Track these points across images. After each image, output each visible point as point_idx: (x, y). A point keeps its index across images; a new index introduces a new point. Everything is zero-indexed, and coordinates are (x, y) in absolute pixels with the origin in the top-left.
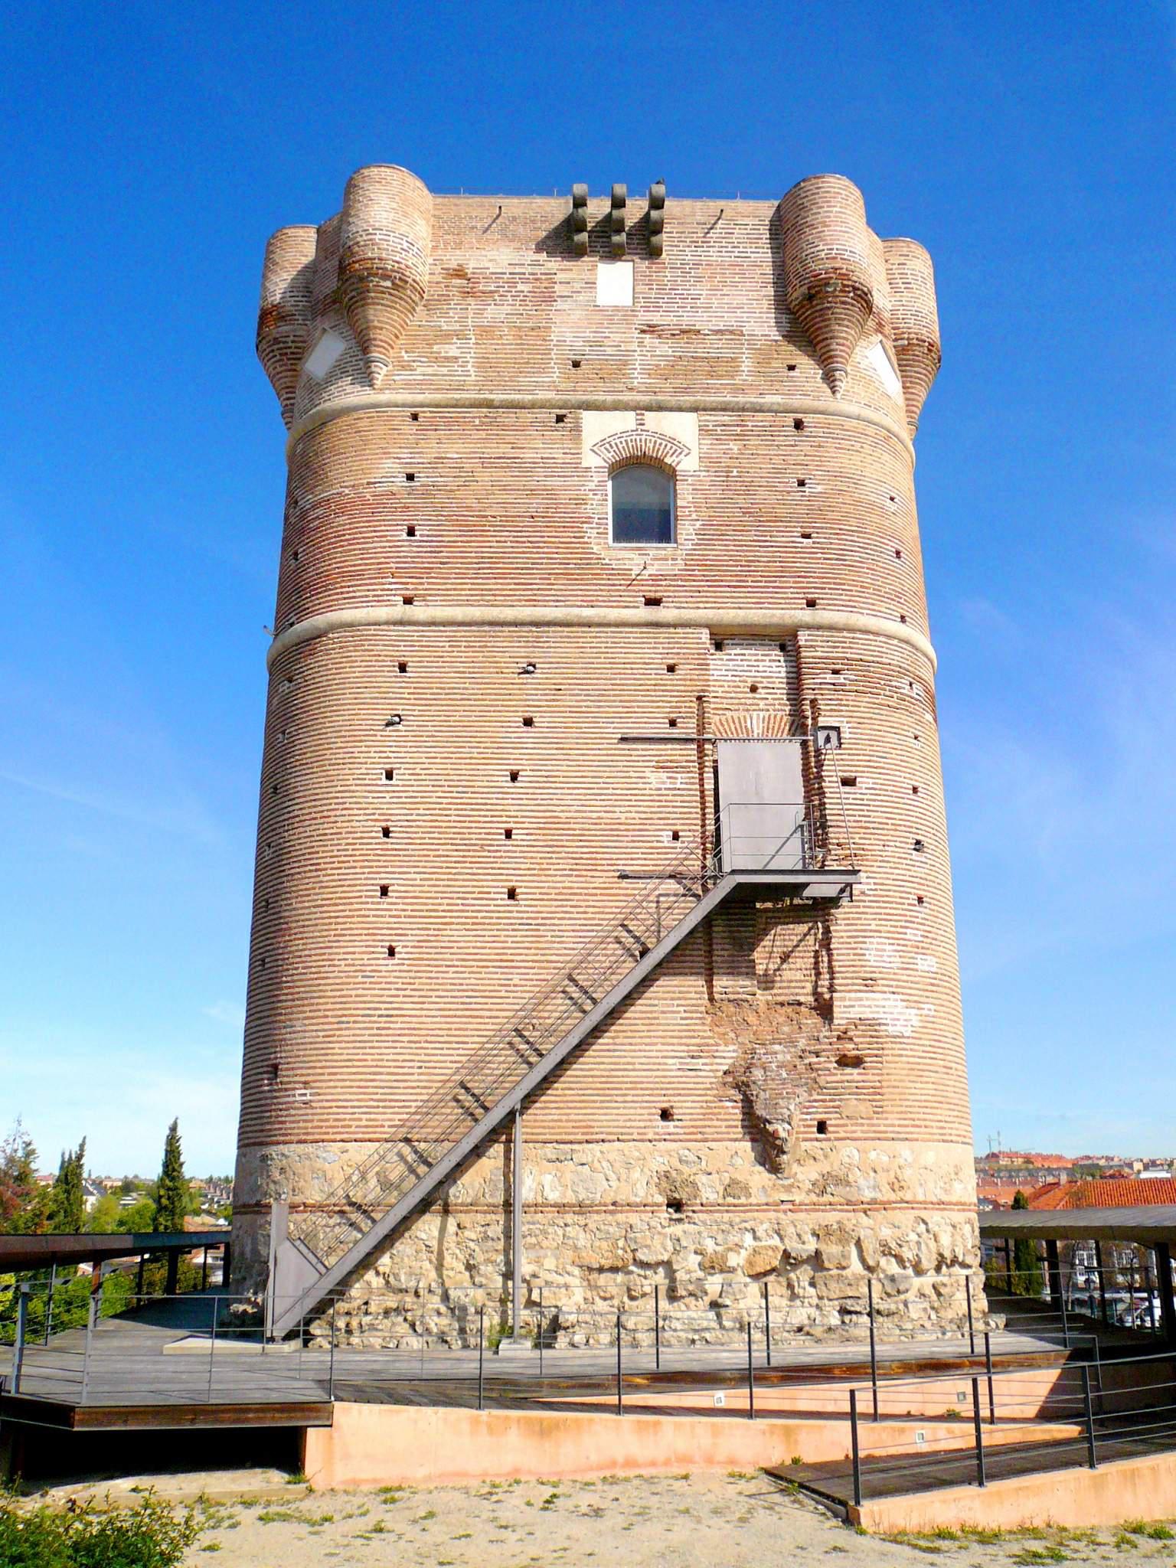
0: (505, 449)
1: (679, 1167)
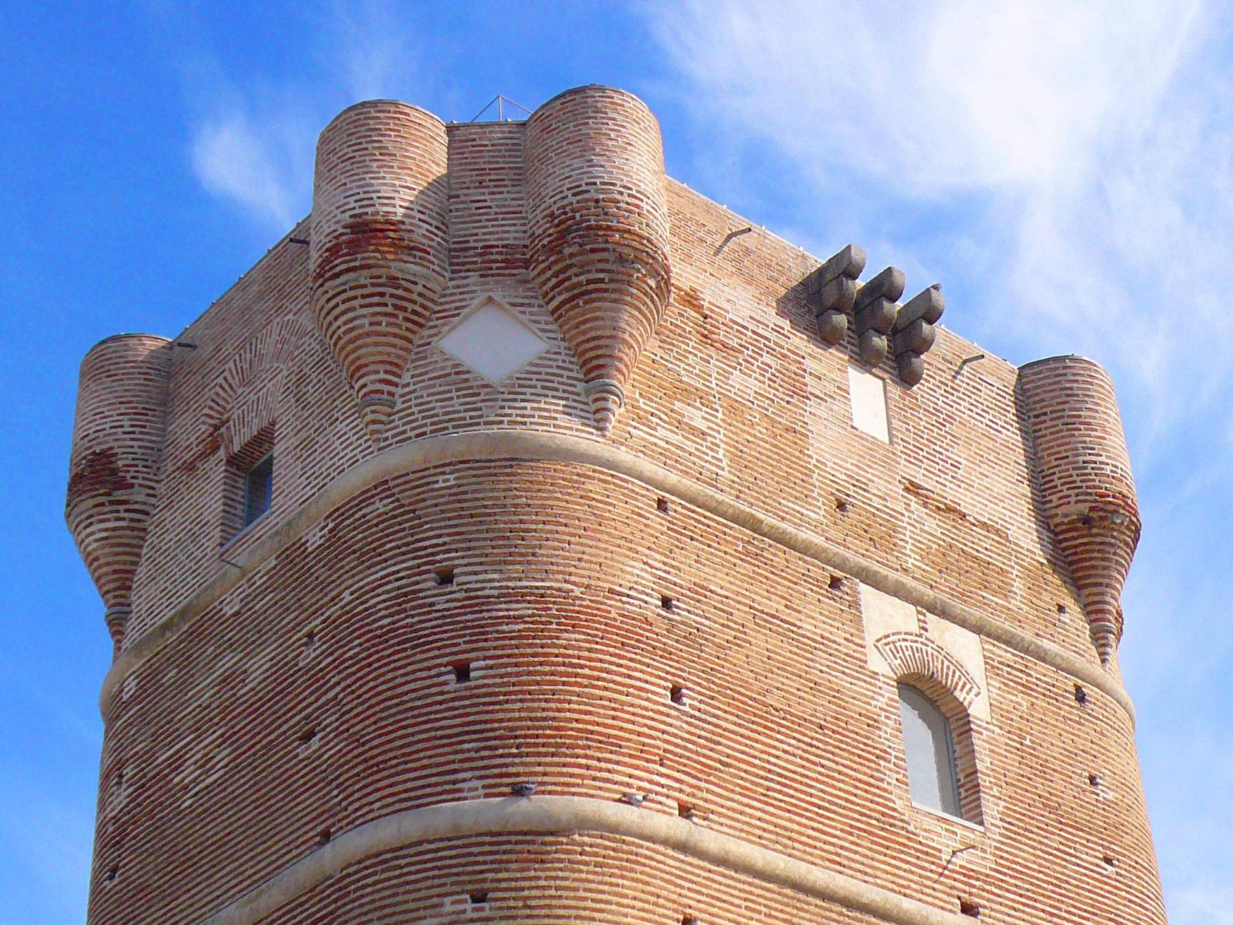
0: (775, 605)
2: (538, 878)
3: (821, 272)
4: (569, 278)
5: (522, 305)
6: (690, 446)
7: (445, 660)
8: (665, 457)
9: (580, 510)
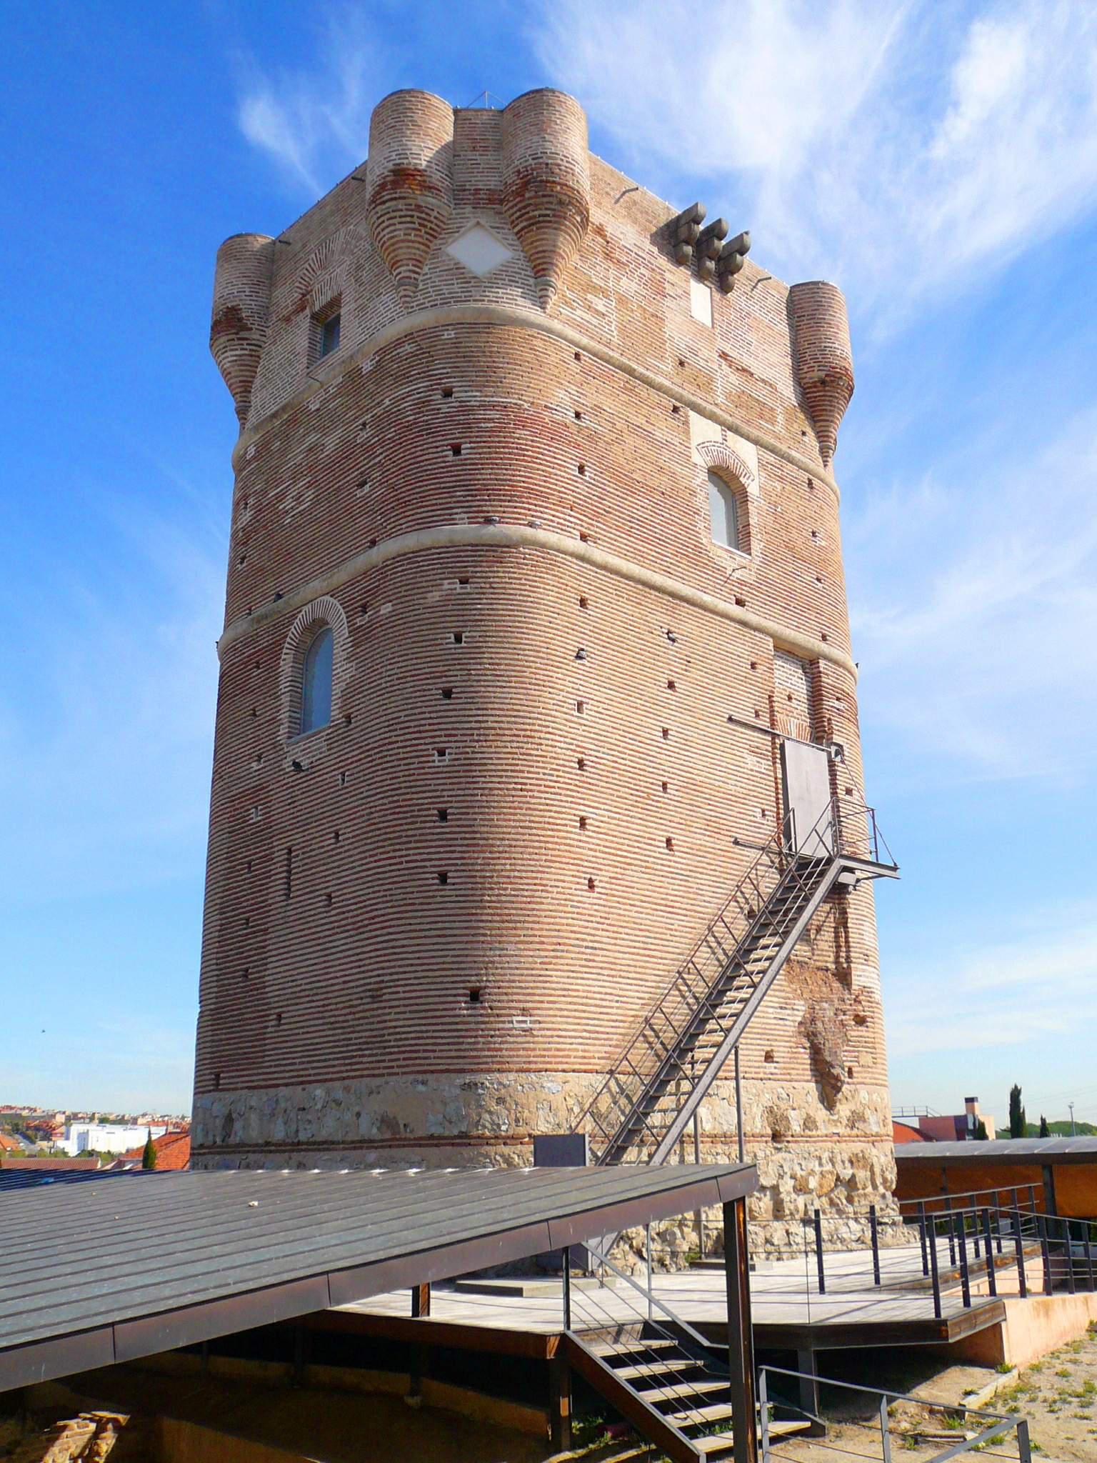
0: (641, 421)
1: (778, 1103)
2: (498, 572)
3: (679, 218)
4: (528, 213)
5: (498, 228)
6: (595, 322)
7: (446, 443)
8: (579, 327)
9: (529, 356)
